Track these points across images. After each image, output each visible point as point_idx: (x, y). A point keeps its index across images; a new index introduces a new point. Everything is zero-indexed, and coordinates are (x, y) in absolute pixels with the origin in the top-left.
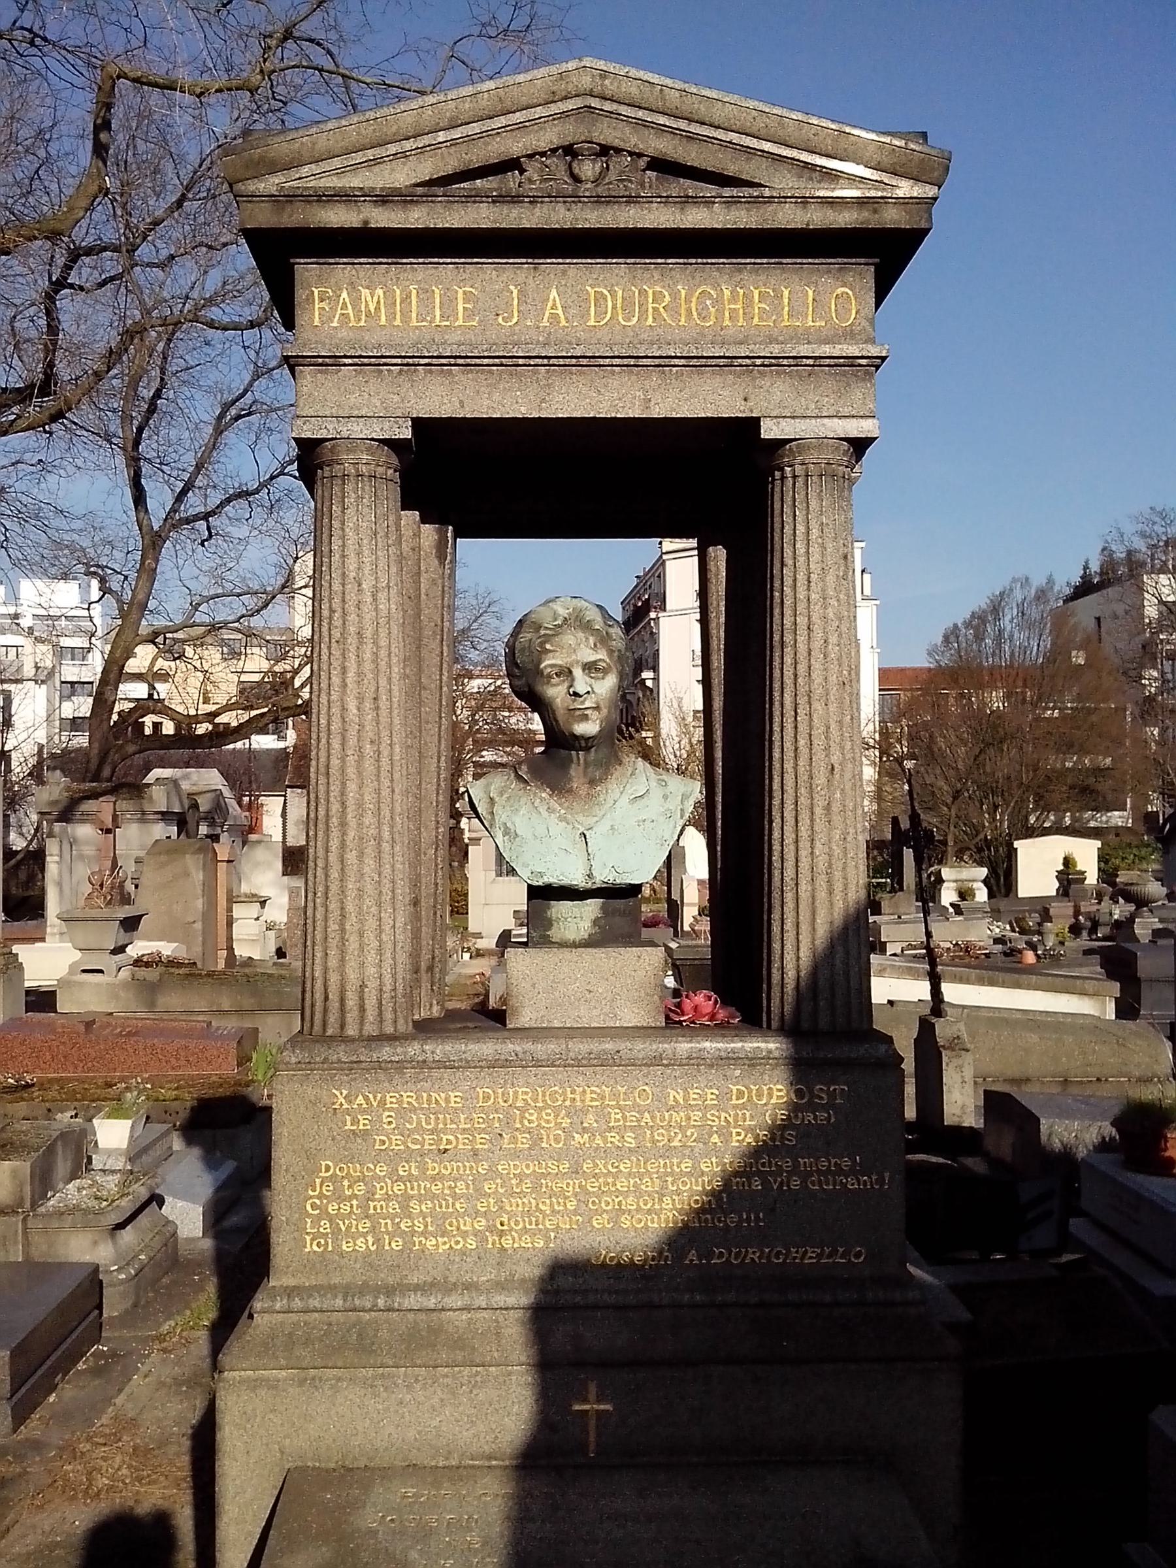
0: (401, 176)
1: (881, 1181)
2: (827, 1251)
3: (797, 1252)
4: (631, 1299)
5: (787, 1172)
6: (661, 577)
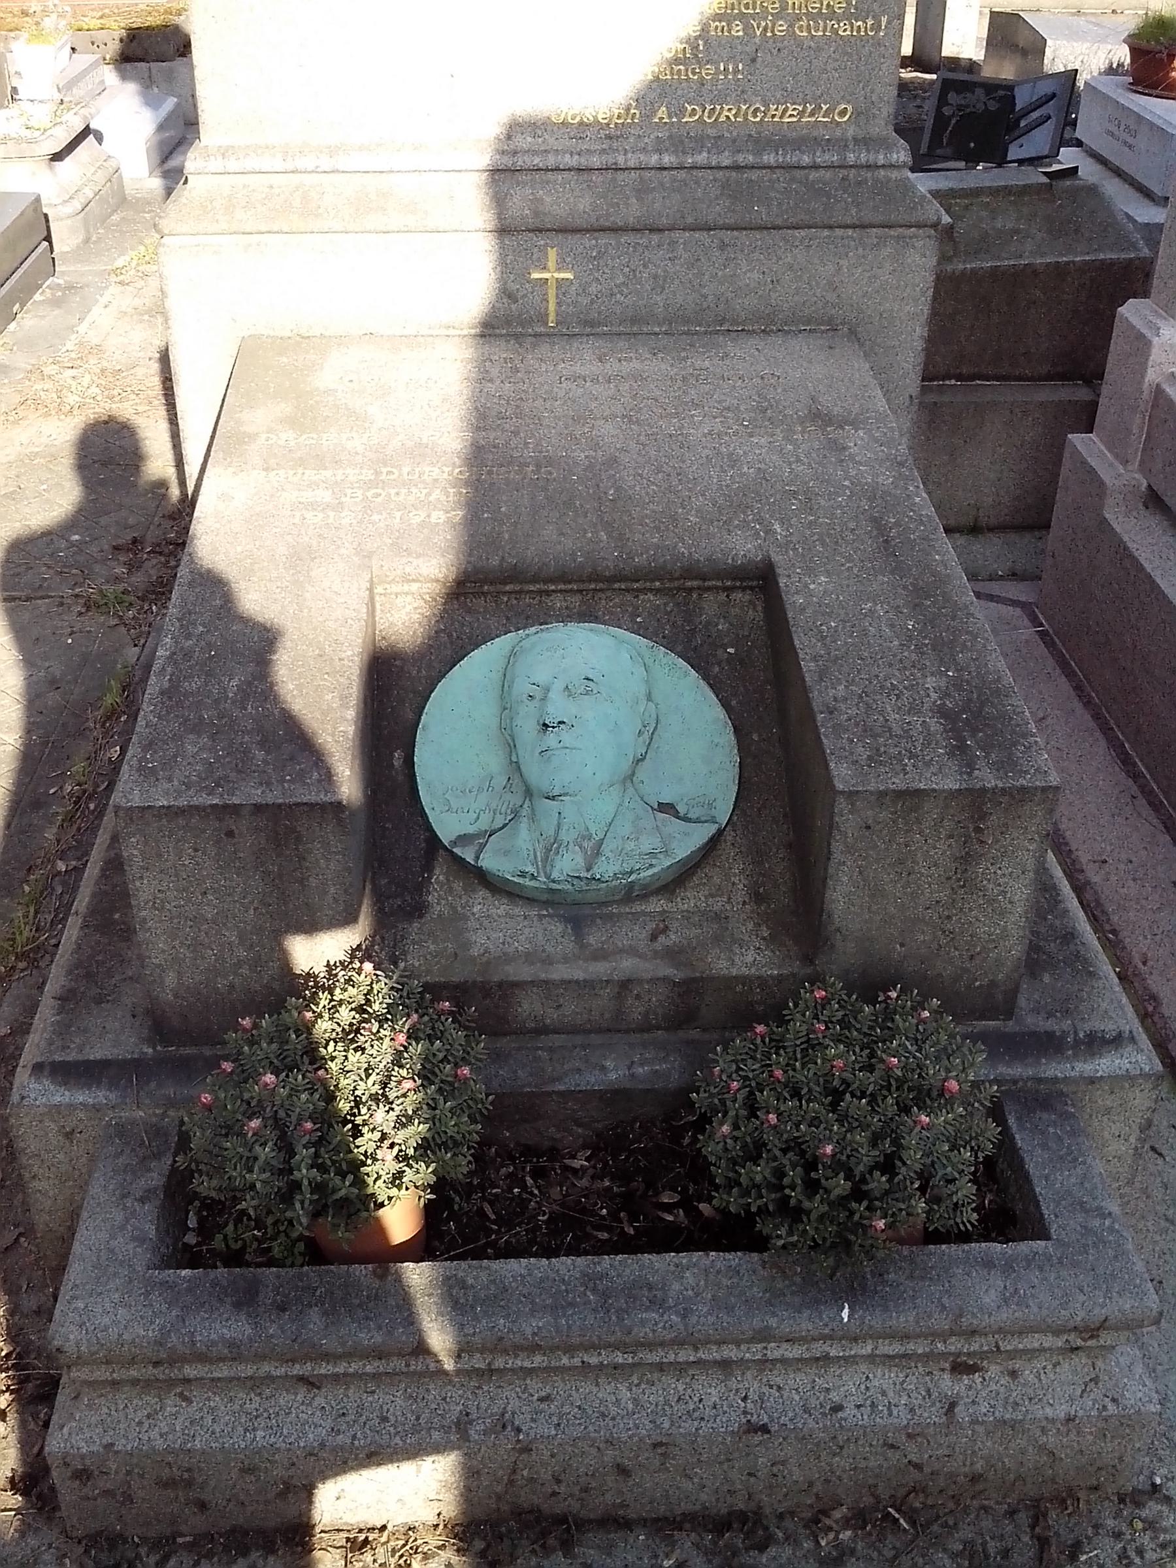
1: (877, 27)
2: (809, 108)
3: (776, 110)
4: (596, 161)
5: (772, 15)
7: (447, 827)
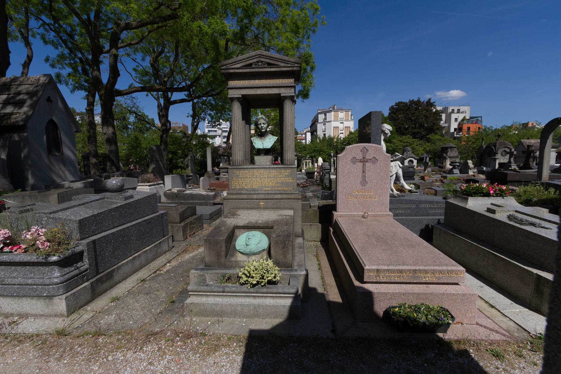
0: (238, 66)
6: (318, 117)
7: (237, 248)
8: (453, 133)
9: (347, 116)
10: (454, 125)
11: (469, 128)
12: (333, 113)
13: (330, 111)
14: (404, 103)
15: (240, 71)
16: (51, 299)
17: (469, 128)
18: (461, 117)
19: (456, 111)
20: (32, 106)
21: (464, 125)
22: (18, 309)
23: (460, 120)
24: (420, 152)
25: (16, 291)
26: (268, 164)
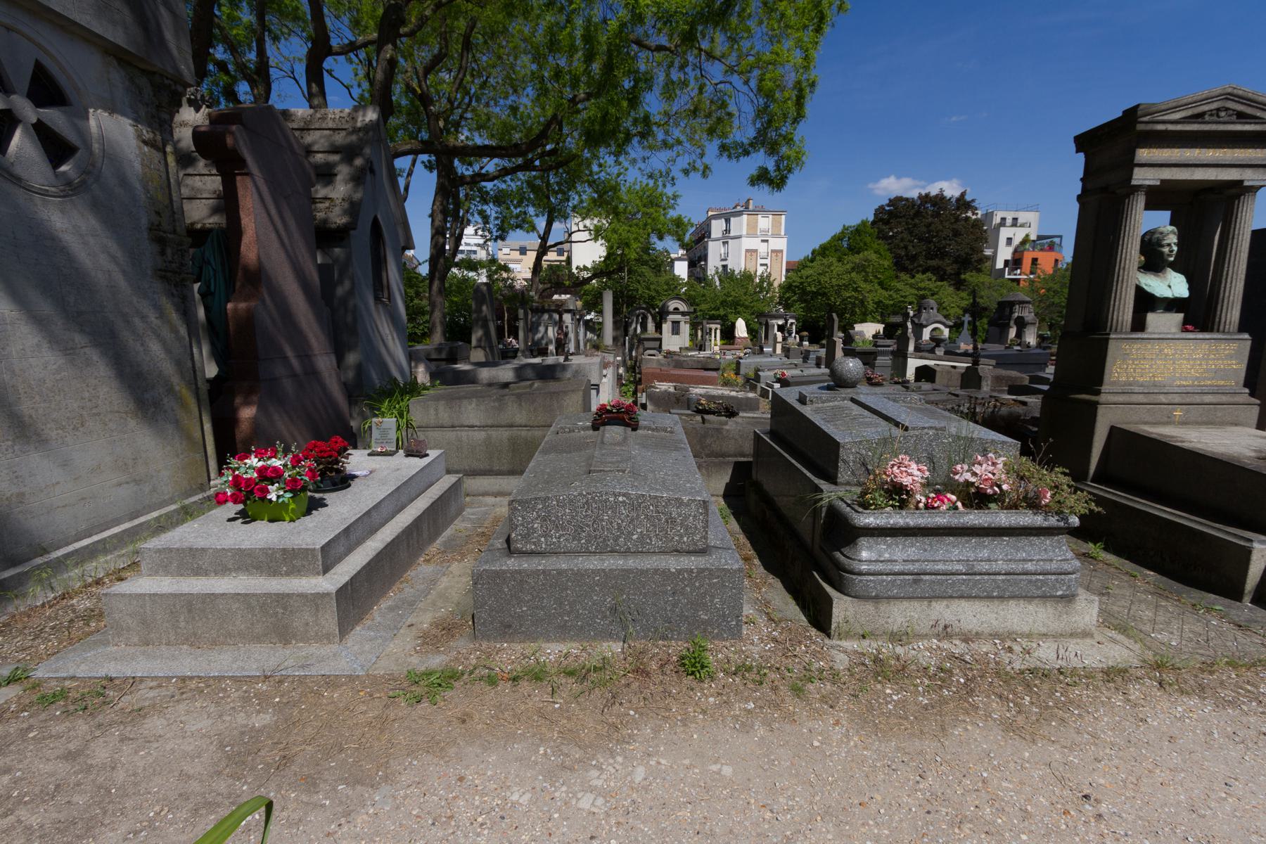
6: (709, 226)
8: (1002, 271)
9: (776, 225)
10: (1004, 254)
11: (1035, 261)
12: (745, 217)
13: (739, 214)
14: (907, 199)
15: (1179, 127)
16: (1070, 601)
17: (1035, 261)
18: (1019, 235)
19: (1009, 222)
20: (357, 179)
21: (1026, 253)
22: (995, 623)
23: (1016, 242)
24: (952, 311)
25: (998, 587)
26: (1174, 330)
